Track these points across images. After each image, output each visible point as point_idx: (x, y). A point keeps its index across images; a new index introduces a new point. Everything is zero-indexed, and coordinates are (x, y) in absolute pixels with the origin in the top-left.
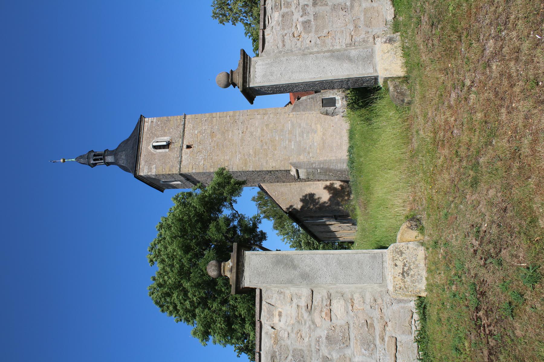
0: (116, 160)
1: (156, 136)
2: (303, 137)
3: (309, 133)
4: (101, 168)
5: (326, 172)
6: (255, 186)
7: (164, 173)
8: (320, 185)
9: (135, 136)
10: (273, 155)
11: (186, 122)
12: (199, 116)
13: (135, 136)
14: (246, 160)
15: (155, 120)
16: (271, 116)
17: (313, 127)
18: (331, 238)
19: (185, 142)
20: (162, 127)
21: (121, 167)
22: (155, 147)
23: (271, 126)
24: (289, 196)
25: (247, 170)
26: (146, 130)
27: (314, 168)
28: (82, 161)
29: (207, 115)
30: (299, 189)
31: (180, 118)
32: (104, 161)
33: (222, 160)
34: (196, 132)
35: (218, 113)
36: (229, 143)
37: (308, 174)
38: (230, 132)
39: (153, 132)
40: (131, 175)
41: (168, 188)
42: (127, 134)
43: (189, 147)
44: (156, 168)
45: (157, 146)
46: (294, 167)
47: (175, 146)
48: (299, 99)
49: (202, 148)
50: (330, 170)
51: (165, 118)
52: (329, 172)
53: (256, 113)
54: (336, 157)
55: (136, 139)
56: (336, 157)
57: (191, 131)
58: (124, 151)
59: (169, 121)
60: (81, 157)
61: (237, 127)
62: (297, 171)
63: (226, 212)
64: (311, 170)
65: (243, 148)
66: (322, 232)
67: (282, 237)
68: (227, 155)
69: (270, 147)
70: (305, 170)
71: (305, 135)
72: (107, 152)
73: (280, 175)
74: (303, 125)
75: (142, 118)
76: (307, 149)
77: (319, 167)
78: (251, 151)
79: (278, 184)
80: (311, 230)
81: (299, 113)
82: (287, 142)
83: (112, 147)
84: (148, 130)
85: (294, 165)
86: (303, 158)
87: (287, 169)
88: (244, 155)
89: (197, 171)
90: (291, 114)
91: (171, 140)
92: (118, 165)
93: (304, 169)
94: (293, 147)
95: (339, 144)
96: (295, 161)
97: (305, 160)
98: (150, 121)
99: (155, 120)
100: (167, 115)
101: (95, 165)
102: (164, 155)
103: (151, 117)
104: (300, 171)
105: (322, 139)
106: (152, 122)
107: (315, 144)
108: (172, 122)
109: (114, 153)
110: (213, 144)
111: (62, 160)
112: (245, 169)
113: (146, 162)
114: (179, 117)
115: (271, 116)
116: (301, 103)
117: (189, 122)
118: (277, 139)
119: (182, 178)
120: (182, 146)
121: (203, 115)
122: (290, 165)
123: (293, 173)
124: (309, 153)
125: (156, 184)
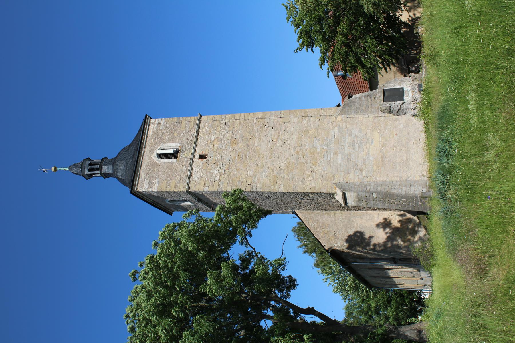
0: (114, 170)
1: (162, 142)
2: (354, 149)
3: (362, 142)
4: (97, 180)
5: (384, 199)
6: (289, 213)
7: (168, 190)
8: (376, 216)
9: (137, 141)
10: (313, 171)
11: (202, 125)
12: (218, 117)
13: (137, 141)
14: (275, 177)
15: (162, 122)
16: (313, 119)
17: (369, 134)
18: (385, 284)
19: (197, 151)
20: (171, 130)
21: (120, 180)
22: (160, 156)
23: (311, 132)
24: (334, 230)
25: (276, 190)
26: (150, 133)
27: (368, 192)
28: (75, 170)
29: (229, 116)
30: (346, 220)
31: (193, 119)
32: (101, 173)
33: (243, 176)
34: (213, 138)
35: (243, 115)
36: (253, 154)
37: (359, 200)
38: (257, 139)
39: (160, 136)
40: (128, 190)
41: (178, 210)
42: (129, 139)
43: (202, 157)
44: (159, 183)
45: (163, 154)
46: (340, 189)
47: (185, 156)
48: (350, 97)
49: (219, 160)
50: (391, 196)
51: (175, 119)
52: (390, 198)
53: (292, 115)
54: (400, 177)
55: (138, 144)
56: (400, 177)
57: (207, 137)
58: (124, 160)
59: (180, 123)
60: (75, 165)
61: (266, 134)
62: (344, 195)
63: (236, 252)
64: (363, 194)
65: (273, 161)
66: (375, 277)
67: (324, 277)
68: (250, 170)
69: (308, 161)
70: (356, 194)
71: (357, 146)
72: (105, 161)
73: (320, 200)
74: (355, 132)
75: (147, 118)
76: (360, 164)
77: (375, 190)
78: (283, 164)
79: (319, 211)
80: (361, 273)
81: (350, 116)
82: (332, 154)
83: (112, 155)
84: (153, 134)
85: (339, 185)
86: (353, 177)
87: (330, 191)
88: (273, 170)
89: (211, 189)
90: (340, 117)
91: (181, 147)
92: (117, 178)
93: (355, 192)
94: (339, 162)
95: (405, 159)
96: (342, 180)
97: (356, 180)
98: (157, 122)
99: (162, 122)
100: (178, 116)
101: (90, 176)
102: (170, 167)
103: (159, 118)
104: (348, 195)
105: (381, 151)
106: (159, 124)
107: (371, 158)
108: (183, 125)
109: (113, 162)
110: (233, 154)
111: (53, 169)
112: (273, 189)
113: (147, 174)
114: (193, 118)
115: (313, 119)
116: (353, 102)
117: (204, 125)
118: (319, 150)
119: (192, 198)
120: (194, 156)
121: (223, 116)
122: (334, 186)
123: (339, 198)
124: (361, 171)
125: (157, 202)
